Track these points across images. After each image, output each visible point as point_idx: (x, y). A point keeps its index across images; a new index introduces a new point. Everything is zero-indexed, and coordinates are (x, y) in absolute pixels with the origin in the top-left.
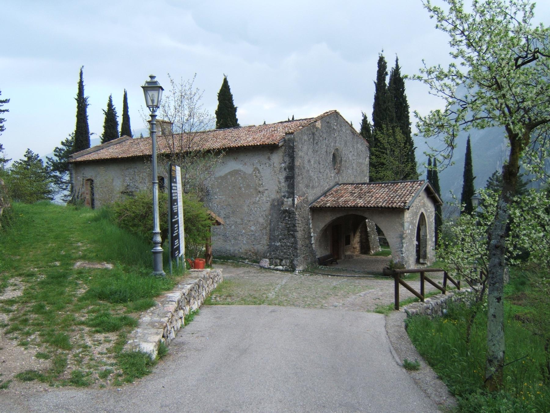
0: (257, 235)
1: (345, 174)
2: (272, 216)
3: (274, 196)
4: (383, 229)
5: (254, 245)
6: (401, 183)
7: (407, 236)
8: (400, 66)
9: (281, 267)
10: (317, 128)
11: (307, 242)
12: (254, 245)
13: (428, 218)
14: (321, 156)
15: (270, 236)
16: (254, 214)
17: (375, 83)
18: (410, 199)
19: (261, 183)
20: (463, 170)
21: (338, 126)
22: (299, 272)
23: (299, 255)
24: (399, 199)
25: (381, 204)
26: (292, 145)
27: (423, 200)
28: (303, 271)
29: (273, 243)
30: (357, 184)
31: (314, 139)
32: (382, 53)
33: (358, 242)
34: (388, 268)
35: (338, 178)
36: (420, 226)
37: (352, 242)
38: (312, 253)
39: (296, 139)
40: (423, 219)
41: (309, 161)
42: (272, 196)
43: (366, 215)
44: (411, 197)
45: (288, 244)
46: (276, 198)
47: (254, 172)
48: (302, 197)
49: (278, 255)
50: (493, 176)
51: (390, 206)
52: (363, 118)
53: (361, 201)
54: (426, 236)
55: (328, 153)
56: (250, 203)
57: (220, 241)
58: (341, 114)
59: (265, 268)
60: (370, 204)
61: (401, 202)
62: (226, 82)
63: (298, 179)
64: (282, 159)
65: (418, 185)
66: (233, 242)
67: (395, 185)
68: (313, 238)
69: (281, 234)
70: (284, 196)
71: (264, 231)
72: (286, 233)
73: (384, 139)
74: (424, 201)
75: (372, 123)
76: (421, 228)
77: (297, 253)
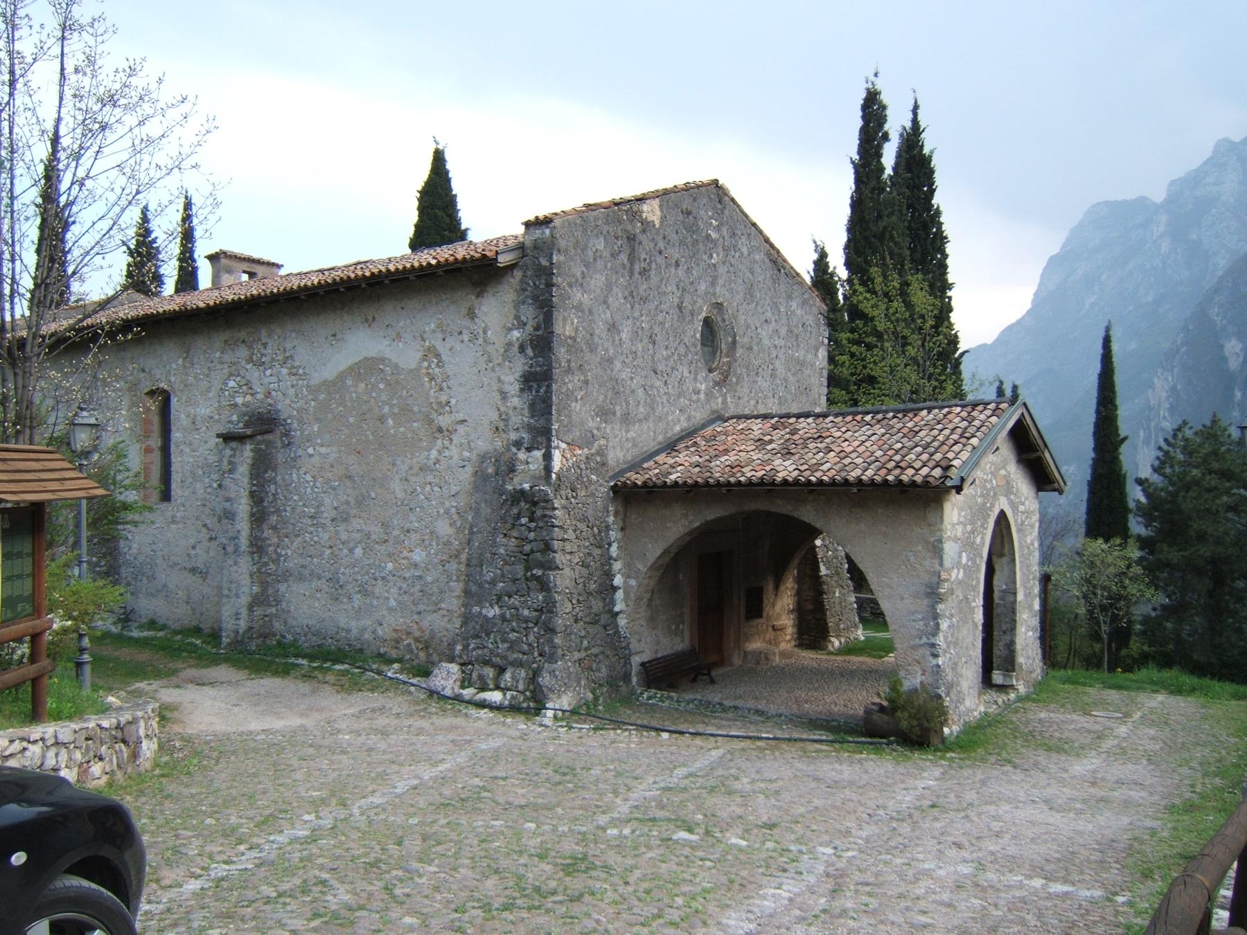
0: (429, 579)
1: (746, 390)
2: (477, 512)
3: (485, 443)
4: (864, 565)
5: (419, 613)
6: (930, 410)
7: (951, 592)
8: (923, 124)
9: (495, 697)
10: (647, 225)
11: (597, 605)
12: (419, 613)
13: (1019, 531)
14: (660, 318)
15: (467, 582)
16: (422, 507)
17: (853, 162)
18: (965, 455)
19: (444, 398)
20: (1092, 418)
21: (724, 230)
22: (555, 717)
23: (560, 652)
24: (925, 457)
25: (858, 472)
26: (544, 262)
27: (1004, 468)
28: (574, 712)
29: (476, 609)
30: (781, 417)
31: (632, 258)
32: (873, 79)
33: (178, 677)
34: (882, 709)
35: (720, 400)
36: (995, 559)
37: (767, 609)
38: (616, 645)
39: (562, 243)
40: (1002, 537)
41: (613, 328)
42: (480, 443)
43: (807, 514)
44: (969, 448)
45: (526, 612)
46: (490, 448)
47: (426, 364)
48: (580, 448)
49: (491, 651)
50: (1175, 436)
51: (890, 478)
52: (815, 256)
53: (787, 463)
54: (1015, 594)
55: (687, 312)
56: (411, 468)
57: (318, 599)
58: (733, 194)
59: (440, 697)
60: (818, 474)
61: (931, 464)
62: (439, 159)
63: (565, 384)
64: (514, 312)
65: (988, 412)
66: (356, 604)
67: (911, 415)
68: (619, 595)
69: (503, 576)
70: (518, 444)
71: (453, 566)
72: (520, 574)
73: (875, 306)
74: (1009, 473)
75: (843, 273)
76: (997, 567)
77: (554, 647)
